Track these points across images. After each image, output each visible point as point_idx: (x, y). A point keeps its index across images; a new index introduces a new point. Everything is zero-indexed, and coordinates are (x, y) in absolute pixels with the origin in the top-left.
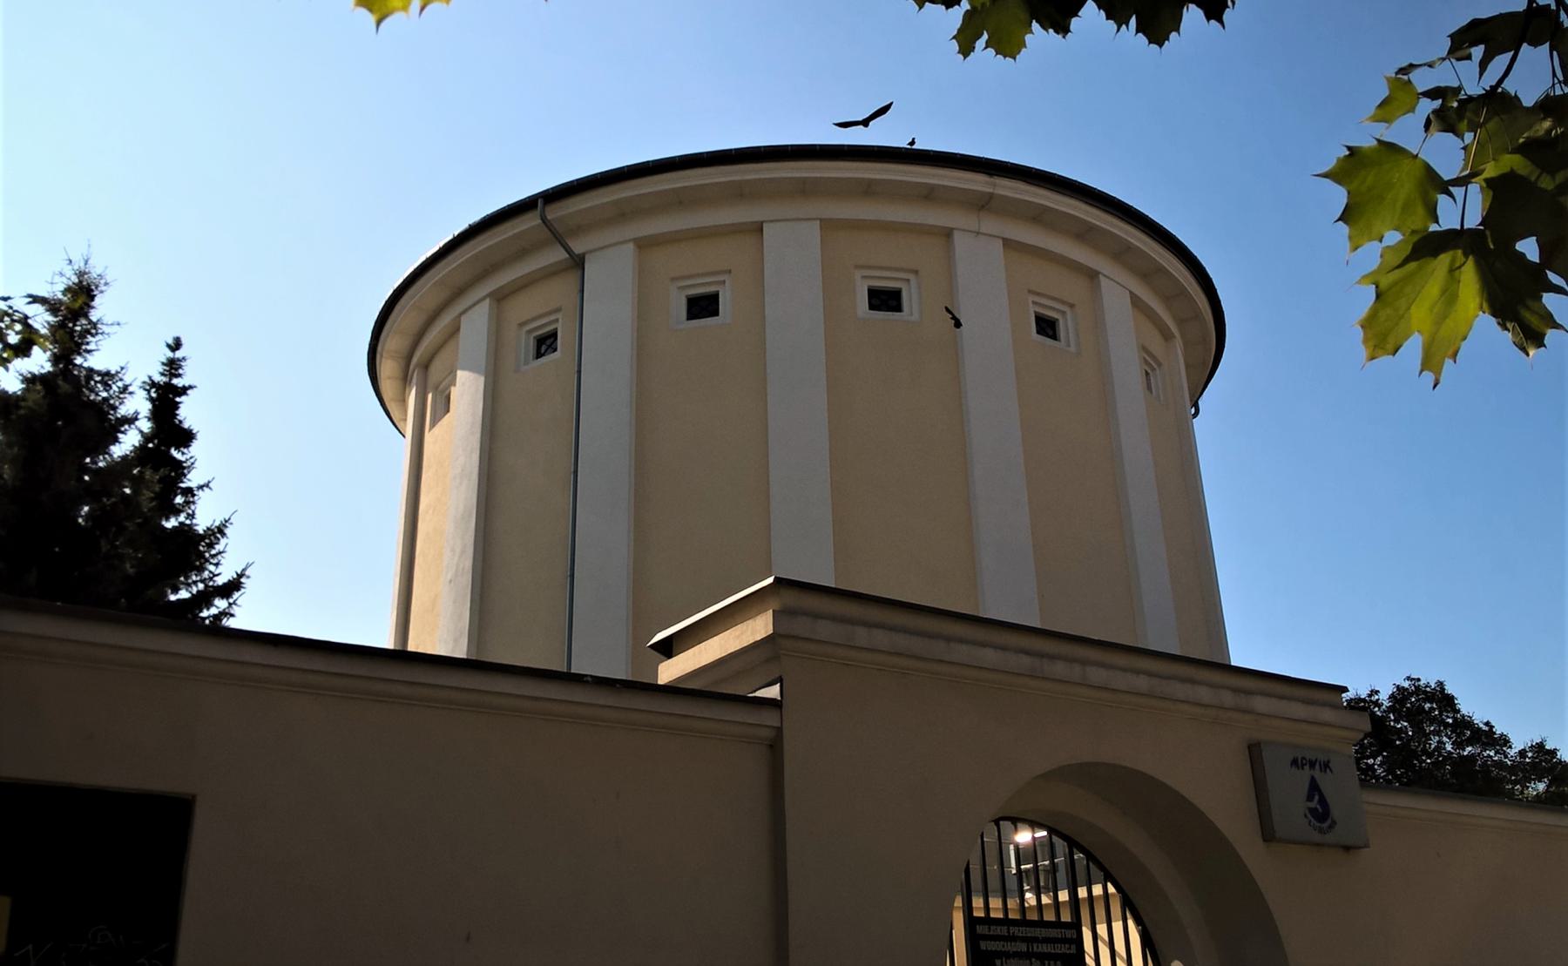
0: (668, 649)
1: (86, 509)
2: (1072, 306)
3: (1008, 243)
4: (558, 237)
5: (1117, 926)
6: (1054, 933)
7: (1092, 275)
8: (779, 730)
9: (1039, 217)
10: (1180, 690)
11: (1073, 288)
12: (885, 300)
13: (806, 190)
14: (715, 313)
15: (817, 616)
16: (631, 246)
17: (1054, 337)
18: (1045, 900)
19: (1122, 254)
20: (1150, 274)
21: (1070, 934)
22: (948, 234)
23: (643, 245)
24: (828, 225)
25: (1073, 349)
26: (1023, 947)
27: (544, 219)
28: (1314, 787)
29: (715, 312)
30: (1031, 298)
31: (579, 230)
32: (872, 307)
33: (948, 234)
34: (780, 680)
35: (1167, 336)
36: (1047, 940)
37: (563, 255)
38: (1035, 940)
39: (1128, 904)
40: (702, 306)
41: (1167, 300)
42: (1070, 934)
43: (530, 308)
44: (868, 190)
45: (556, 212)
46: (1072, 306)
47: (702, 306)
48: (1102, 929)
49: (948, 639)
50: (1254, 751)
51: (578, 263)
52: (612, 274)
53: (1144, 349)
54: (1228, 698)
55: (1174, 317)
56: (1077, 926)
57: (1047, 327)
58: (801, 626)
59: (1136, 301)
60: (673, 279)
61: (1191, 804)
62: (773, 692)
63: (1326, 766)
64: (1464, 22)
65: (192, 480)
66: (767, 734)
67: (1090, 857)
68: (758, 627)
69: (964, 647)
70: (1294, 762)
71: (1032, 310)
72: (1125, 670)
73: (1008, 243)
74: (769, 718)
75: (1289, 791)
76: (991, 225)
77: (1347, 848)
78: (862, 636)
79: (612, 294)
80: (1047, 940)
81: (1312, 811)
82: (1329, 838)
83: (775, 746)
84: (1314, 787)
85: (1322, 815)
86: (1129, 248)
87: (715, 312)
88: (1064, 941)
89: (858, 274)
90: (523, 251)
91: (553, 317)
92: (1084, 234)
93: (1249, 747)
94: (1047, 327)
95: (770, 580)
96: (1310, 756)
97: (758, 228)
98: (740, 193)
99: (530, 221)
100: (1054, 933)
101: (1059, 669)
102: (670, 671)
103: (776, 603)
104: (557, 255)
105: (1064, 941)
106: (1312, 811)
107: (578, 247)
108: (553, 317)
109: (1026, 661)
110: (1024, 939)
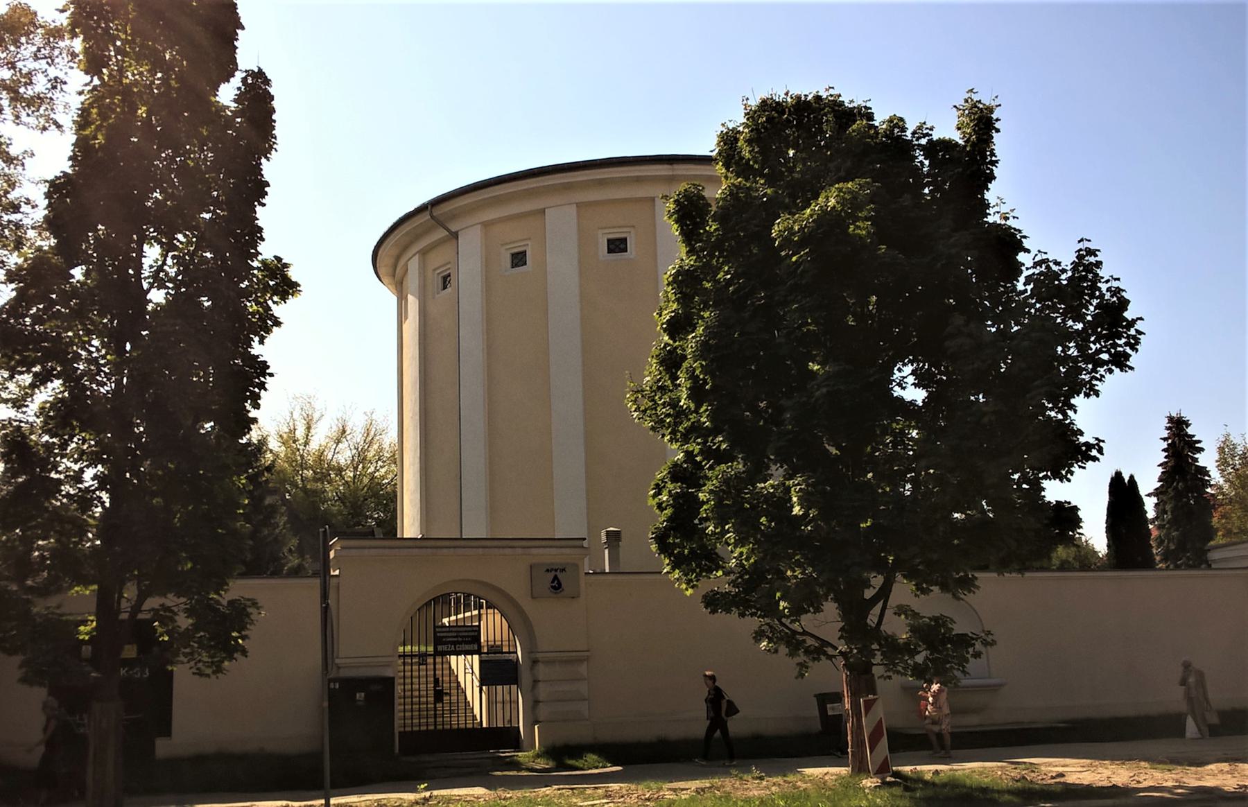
1: (956, 515)
13: (568, 187)
37: (445, 233)
43: (438, 259)
44: (601, 183)
45: (438, 211)
47: (618, 246)
51: (455, 235)
52: (471, 242)
61: (982, 747)
64: (807, 86)
65: (1160, 470)
79: (470, 254)
89: (600, 232)
90: (427, 231)
97: (543, 211)
98: (530, 193)
99: (425, 217)
104: (441, 233)
107: (454, 228)
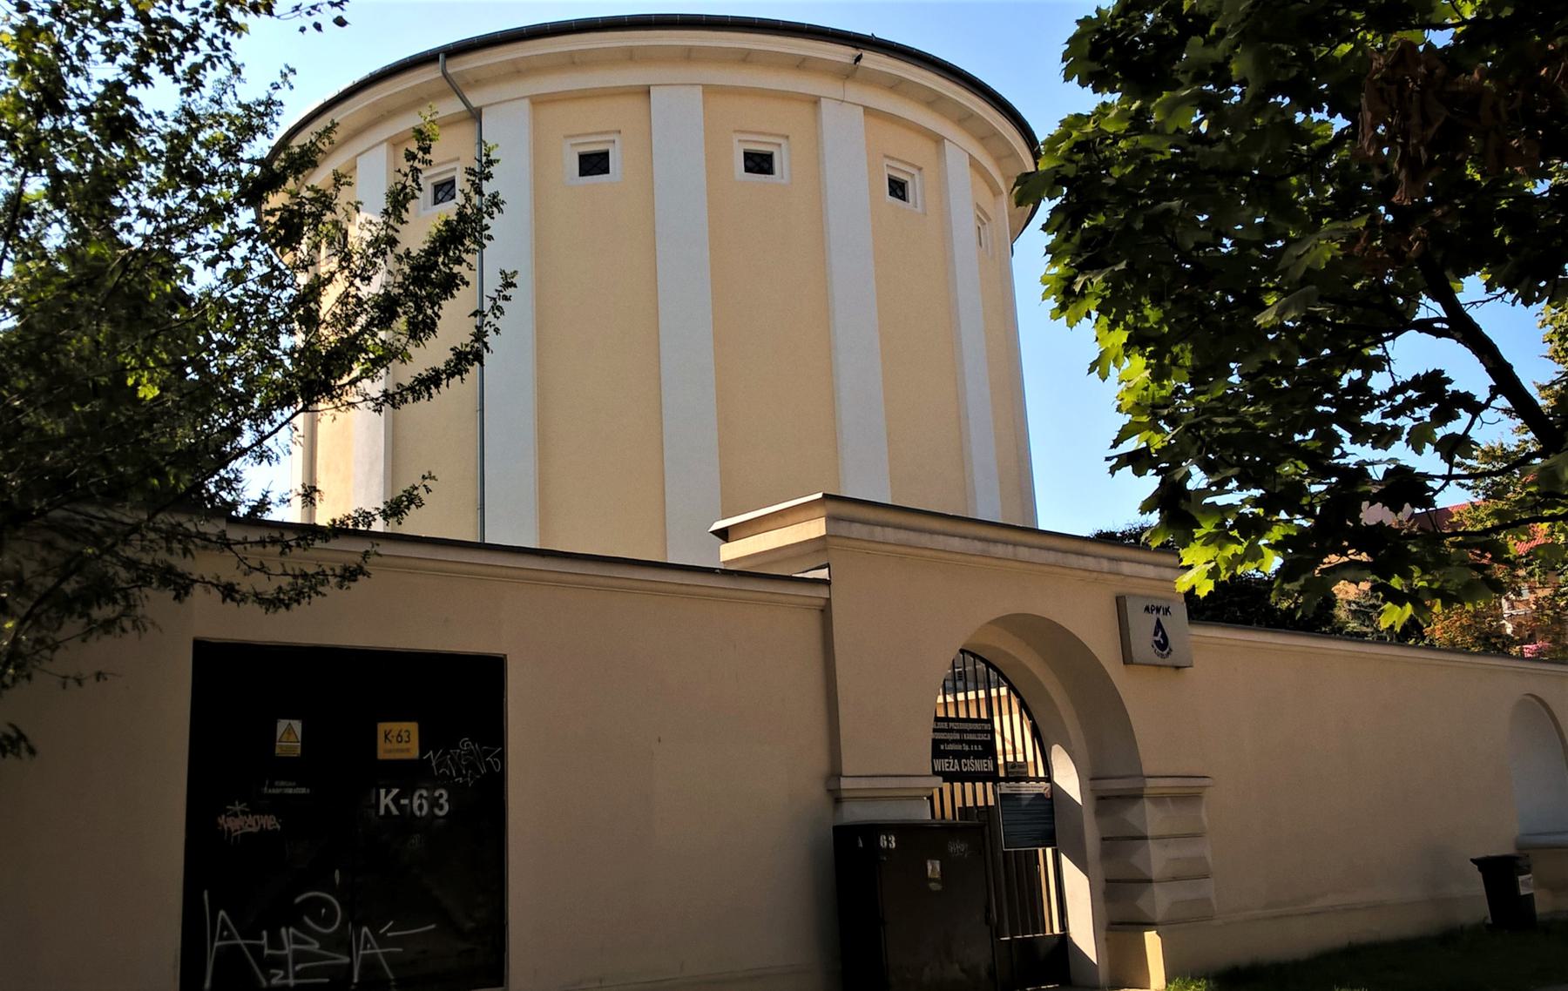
0: (724, 535)
2: (920, 169)
3: (868, 111)
4: (455, 88)
5: (1016, 717)
6: (977, 726)
7: (939, 140)
8: (829, 600)
9: (896, 86)
10: (1073, 560)
11: (919, 150)
12: (759, 163)
13: (689, 56)
14: (606, 171)
15: (852, 521)
16: (527, 102)
17: (903, 198)
18: (950, 699)
19: (964, 119)
20: (987, 137)
21: (987, 727)
22: (815, 101)
23: (537, 101)
24: (709, 90)
25: (919, 209)
26: (957, 736)
27: (445, 75)
28: (1159, 625)
29: (605, 170)
30: (887, 161)
31: (478, 83)
32: (747, 170)
33: (815, 101)
34: (828, 566)
35: (996, 192)
36: (972, 731)
38: (965, 731)
39: (1023, 706)
40: (594, 164)
41: (998, 160)
42: (987, 727)
45: (457, 66)
46: (920, 169)
47: (594, 164)
48: (1006, 718)
49: (932, 532)
50: (1120, 602)
51: (475, 115)
53: (978, 206)
54: (1105, 565)
55: (1003, 175)
56: (990, 721)
57: (898, 188)
58: (843, 529)
59: (974, 164)
60: (566, 137)
62: (823, 574)
63: (1167, 611)
66: (822, 602)
67: (989, 665)
68: (815, 528)
69: (941, 538)
70: (1147, 609)
71: (887, 172)
72: (1040, 548)
73: (868, 111)
74: (823, 592)
75: (1142, 629)
76: (855, 92)
77: (1178, 668)
78: (878, 532)
80: (972, 731)
81: (1157, 643)
82: (1168, 661)
83: (826, 611)
84: (1159, 625)
85: (1163, 645)
86: (996, 134)
87: (605, 170)
88: (983, 731)
91: (451, 166)
92: (934, 102)
93: (1117, 599)
94: (898, 188)
95: (820, 495)
96: (1157, 603)
99: (430, 74)
100: (977, 726)
101: (999, 550)
102: (730, 552)
103: (821, 511)
104: (453, 106)
105: (983, 731)
106: (1157, 643)
107: (475, 99)
108: (451, 166)
109: (979, 545)
110: (959, 731)
